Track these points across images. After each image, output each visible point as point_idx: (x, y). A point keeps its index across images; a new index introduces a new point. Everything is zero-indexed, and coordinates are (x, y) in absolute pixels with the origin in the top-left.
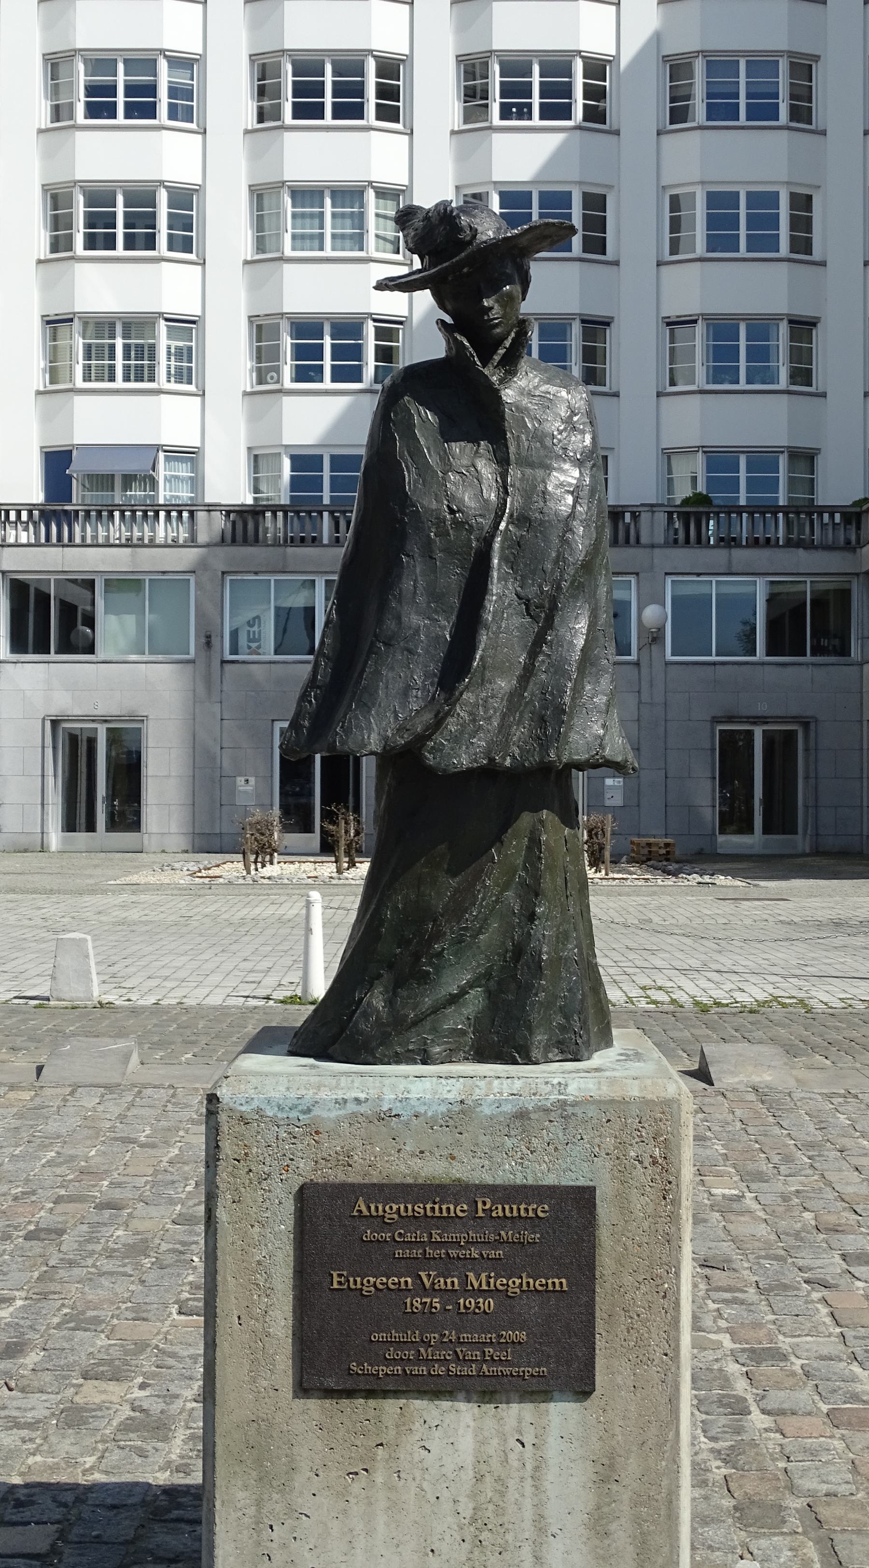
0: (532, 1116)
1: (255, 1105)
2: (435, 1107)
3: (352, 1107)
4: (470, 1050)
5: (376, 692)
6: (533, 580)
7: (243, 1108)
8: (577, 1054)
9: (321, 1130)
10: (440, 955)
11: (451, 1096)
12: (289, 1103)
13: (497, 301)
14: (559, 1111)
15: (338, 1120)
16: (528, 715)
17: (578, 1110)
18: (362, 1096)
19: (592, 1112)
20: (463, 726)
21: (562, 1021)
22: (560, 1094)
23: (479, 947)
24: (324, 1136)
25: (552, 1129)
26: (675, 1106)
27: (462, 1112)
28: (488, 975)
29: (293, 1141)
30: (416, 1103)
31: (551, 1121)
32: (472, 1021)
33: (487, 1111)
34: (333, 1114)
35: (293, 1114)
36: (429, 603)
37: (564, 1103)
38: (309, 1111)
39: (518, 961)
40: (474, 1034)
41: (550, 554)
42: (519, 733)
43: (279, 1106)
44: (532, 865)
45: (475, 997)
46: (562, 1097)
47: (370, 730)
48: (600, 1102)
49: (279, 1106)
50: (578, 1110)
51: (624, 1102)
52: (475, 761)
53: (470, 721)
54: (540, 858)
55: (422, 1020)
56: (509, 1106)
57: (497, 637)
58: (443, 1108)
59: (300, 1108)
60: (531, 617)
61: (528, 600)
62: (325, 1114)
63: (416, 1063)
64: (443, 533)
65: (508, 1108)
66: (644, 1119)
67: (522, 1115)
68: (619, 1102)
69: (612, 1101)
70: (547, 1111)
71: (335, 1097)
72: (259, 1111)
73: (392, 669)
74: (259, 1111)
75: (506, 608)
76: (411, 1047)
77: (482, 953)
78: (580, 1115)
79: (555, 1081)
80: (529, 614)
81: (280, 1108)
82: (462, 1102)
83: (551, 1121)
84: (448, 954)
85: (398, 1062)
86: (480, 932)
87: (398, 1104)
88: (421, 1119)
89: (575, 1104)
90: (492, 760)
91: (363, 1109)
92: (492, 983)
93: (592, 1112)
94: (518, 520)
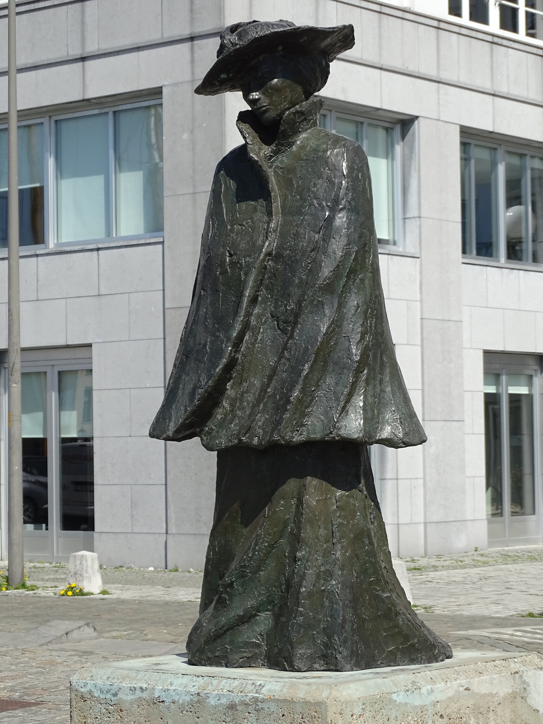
0: (239, 708)
1: (89, 687)
2: (183, 697)
3: (138, 693)
4: (265, 659)
5: (177, 392)
6: (282, 302)
7: (82, 690)
8: (336, 666)
9: (123, 709)
10: (231, 585)
11: (192, 690)
12: (106, 688)
13: (263, 94)
14: (254, 706)
15: (131, 703)
16: (270, 405)
17: (265, 706)
18: (144, 686)
19: (273, 707)
20: (226, 415)
21: (326, 639)
22: (257, 693)
23: (259, 581)
24: (124, 713)
25: (250, 719)
26: (323, 707)
27: (198, 702)
28: (270, 602)
29: (109, 715)
30: (173, 694)
31: (249, 713)
32: (265, 637)
33: (212, 702)
34: (129, 698)
35: (109, 696)
36: (214, 324)
37: (256, 700)
38: (115, 695)
39: (288, 593)
40: (267, 646)
41: (294, 281)
42: (261, 419)
43: (101, 690)
44: (298, 519)
45: (266, 619)
46: (257, 695)
47: (170, 421)
48: (278, 700)
49: (101, 690)
50: (265, 706)
51: (292, 701)
52: (230, 441)
53: (230, 411)
54: (302, 514)
55: (223, 634)
56: (225, 700)
57: (254, 347)
58: (188, 698)
59: (112, 692)
60: (281, 330)
61: (278, 318)
62: (125, 698)
63: (222, 666)
64: (224, 272)
65: (224, 701)
66: (305, 716)
67: (232, 707)
68: (289, 701)
69: (285, 701)
70: (247, 705)
71: (130, 685)
72: (90, 692)
73: (188, 374)
74: (90, 692)
75: (263, 324)
76: (217, 654)
77: (262, 585)
78: (267, 710)
79: (259, 683)
80: (279, 328)
81: (102, 692)
82: (198, 694)
83: (249, 713)
84: (237, 585)
85: (211, 665)
86: (259, 569)
87: (163, 693)
88: (176, 704)
89: (263, 701)
90: (240, 440)
91: (145, 695)
92: (276, 609)
93: (273, 707)
94: (276, 257)
